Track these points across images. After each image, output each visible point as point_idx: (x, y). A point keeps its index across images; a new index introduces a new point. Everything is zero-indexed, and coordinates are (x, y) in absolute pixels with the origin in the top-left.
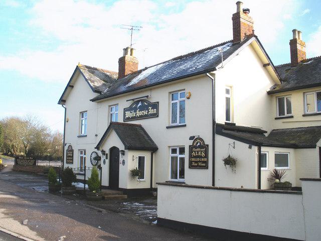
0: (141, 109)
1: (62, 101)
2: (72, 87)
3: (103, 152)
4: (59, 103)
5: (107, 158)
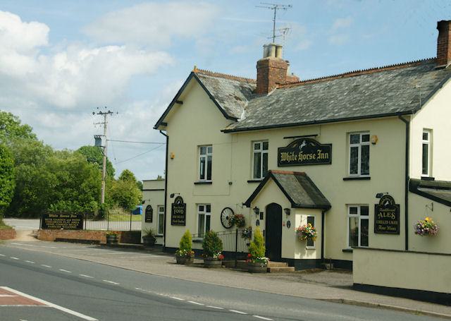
0: (306, 151)
1: (161, 124)
2: (181, 103)
3: (257, 210)
4: (156, 127)
5: (262, 218)
